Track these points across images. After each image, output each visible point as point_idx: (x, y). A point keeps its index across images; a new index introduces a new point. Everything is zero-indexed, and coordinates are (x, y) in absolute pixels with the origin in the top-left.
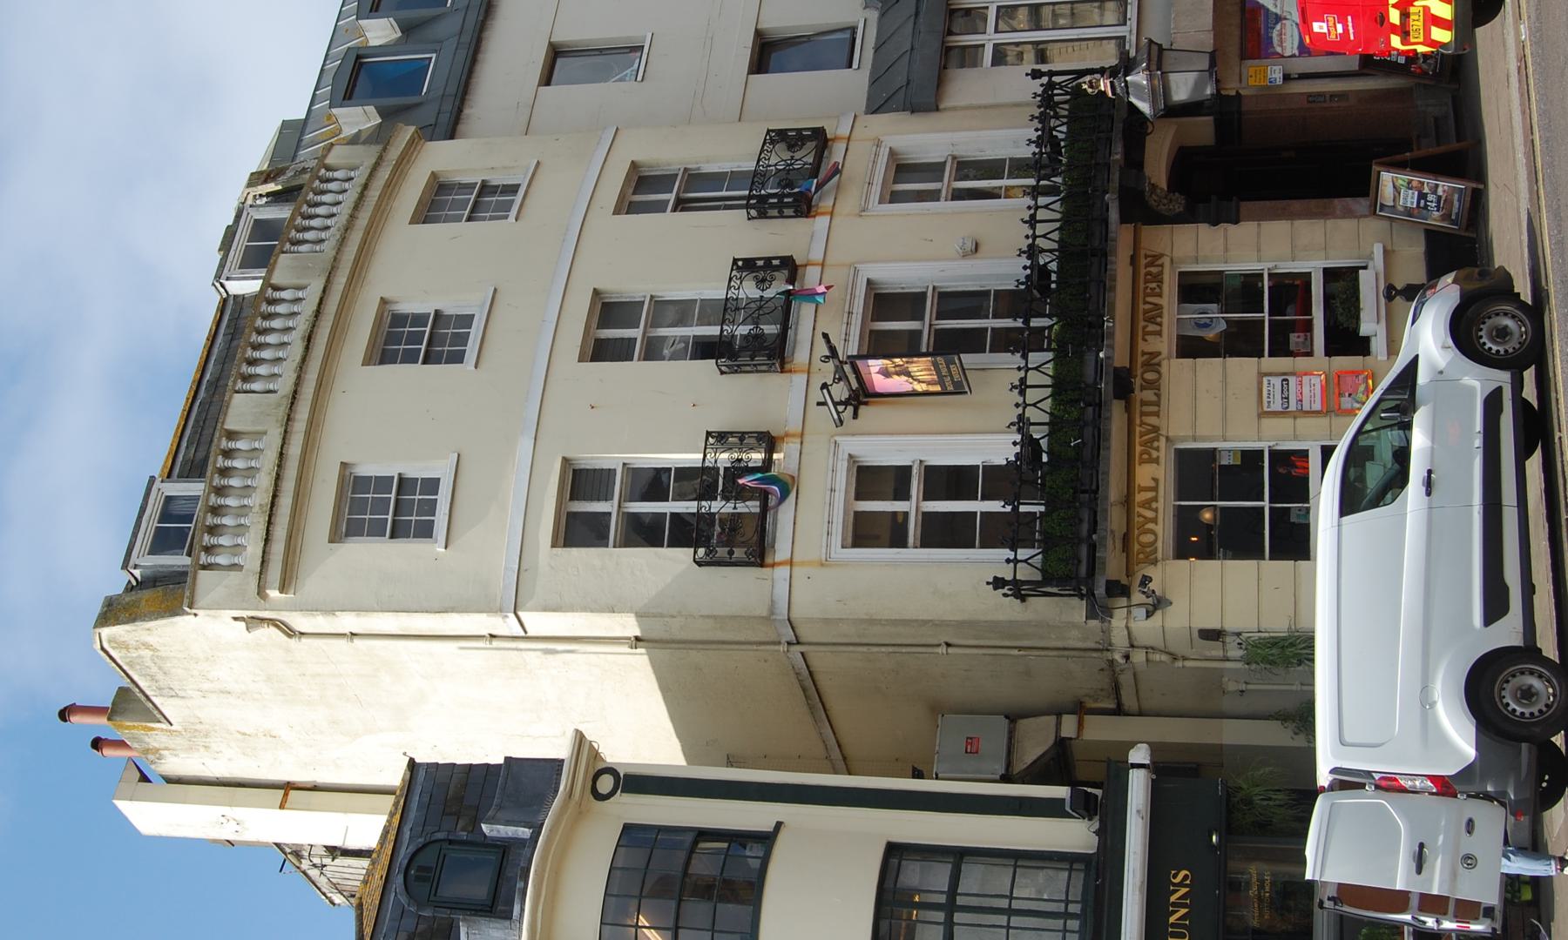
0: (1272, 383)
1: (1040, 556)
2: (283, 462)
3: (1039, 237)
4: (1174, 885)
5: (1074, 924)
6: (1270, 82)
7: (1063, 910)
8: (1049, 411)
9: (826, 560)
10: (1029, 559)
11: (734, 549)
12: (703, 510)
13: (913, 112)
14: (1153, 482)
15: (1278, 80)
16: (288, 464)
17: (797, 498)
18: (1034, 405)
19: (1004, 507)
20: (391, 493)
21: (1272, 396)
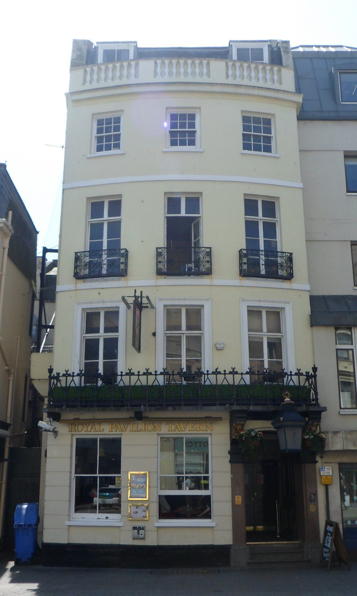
3: (242, 376)
8: (239, 384)
10: (123, 381)
11: (246, 265)
12: (261, 252)
18: (225, 378)
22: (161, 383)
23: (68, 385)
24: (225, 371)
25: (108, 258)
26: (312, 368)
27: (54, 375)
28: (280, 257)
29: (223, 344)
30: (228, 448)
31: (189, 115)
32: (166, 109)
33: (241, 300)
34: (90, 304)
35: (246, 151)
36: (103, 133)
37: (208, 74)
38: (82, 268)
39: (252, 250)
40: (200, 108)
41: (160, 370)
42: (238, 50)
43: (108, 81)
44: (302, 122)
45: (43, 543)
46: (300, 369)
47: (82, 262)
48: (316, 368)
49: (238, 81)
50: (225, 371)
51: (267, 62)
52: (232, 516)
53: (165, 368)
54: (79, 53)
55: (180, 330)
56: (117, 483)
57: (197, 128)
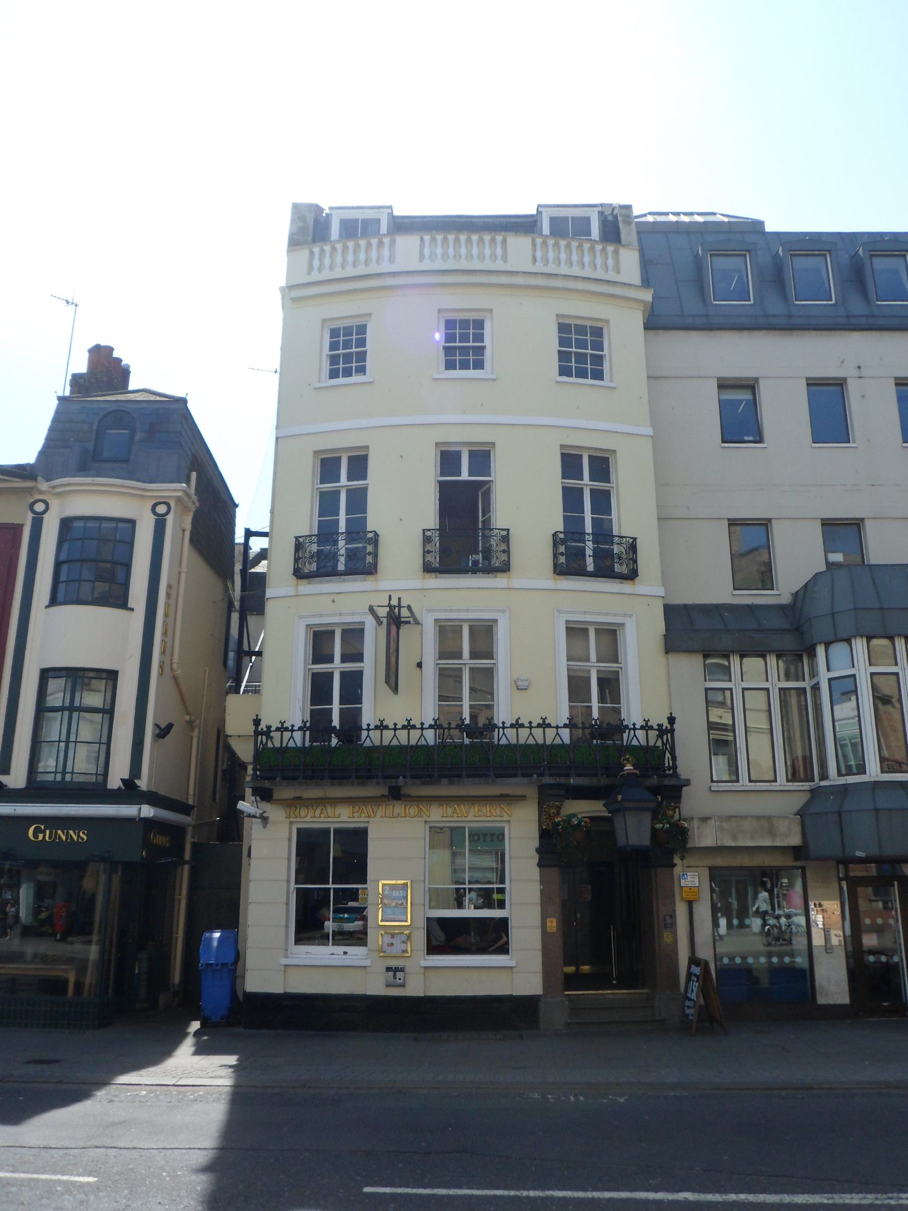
4: (79, 832)
5: (59, 777)
7: (67, 771)
8: (391, 744)
13: (665, 636)
18: (531, 733)
20: (473, 342)
26: (668, 718)
27: (262, 729)
28: (618, 544)
29: (527, 680)
30: (536, 843)
31: (474, 321)
35: (564, 379)
36: (339, 350)
37: (505, 258)
39: (573, 533)
40: (491, 311)
41: (429, 721)
42: (552, 220)
44: (651, 333)
47: (306, 552)
48: (675, 718)
49: (551, 268)
50: (530, 723)
51: (597, 239)
54: (301, 224)
55: (461, 657)
56: (361, 898)
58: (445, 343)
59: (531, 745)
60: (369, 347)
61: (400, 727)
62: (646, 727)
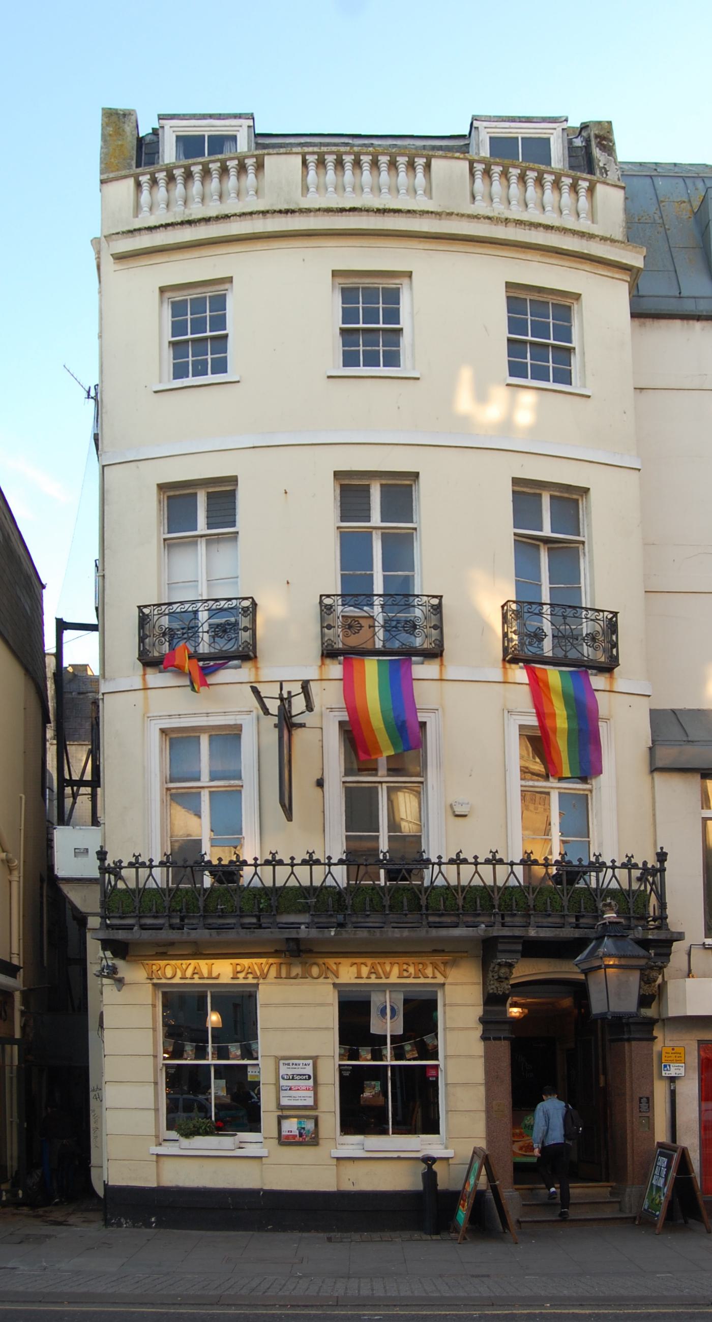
0: (307, 1067)
1: (155, 886)
2: (222, 220)
6: (665, 1066)
8: (287, 885)
9: (148, 717)
14: (217, 974)
15: (668, 1072)
16: (222, 225)
17: (179, 687)
18: (476, 872)
19: (594, 855)
21: (294, 1066)
22: (342, 882)
23: (141, 886)
24: (476, 857)
25: (212, 621)
27: (109, 864)
28: (592, 620)
29: (468, 804)
32: (333, 276)
33: (506, 712)
34: (205, 718)
36: (206, 332)
37: (428, 192)
38: (157, 640)
40: (409, 275)
43: (229, 201)
45: (106, 1186)
46: (632, 856)
47: (154, 627)
48: (666, 854)
50: (476, 857)
52: (486, 1138)
53: (563, 853)
56: (251, 1075)
57: (405, 321)
58: (343, 323)
59: (514, 887)
60: (230, 329)
61: (300, 862)
62: (629, 865)
